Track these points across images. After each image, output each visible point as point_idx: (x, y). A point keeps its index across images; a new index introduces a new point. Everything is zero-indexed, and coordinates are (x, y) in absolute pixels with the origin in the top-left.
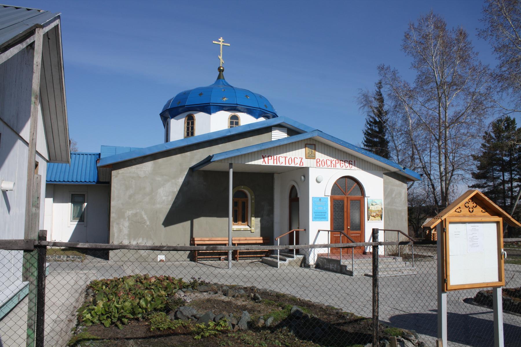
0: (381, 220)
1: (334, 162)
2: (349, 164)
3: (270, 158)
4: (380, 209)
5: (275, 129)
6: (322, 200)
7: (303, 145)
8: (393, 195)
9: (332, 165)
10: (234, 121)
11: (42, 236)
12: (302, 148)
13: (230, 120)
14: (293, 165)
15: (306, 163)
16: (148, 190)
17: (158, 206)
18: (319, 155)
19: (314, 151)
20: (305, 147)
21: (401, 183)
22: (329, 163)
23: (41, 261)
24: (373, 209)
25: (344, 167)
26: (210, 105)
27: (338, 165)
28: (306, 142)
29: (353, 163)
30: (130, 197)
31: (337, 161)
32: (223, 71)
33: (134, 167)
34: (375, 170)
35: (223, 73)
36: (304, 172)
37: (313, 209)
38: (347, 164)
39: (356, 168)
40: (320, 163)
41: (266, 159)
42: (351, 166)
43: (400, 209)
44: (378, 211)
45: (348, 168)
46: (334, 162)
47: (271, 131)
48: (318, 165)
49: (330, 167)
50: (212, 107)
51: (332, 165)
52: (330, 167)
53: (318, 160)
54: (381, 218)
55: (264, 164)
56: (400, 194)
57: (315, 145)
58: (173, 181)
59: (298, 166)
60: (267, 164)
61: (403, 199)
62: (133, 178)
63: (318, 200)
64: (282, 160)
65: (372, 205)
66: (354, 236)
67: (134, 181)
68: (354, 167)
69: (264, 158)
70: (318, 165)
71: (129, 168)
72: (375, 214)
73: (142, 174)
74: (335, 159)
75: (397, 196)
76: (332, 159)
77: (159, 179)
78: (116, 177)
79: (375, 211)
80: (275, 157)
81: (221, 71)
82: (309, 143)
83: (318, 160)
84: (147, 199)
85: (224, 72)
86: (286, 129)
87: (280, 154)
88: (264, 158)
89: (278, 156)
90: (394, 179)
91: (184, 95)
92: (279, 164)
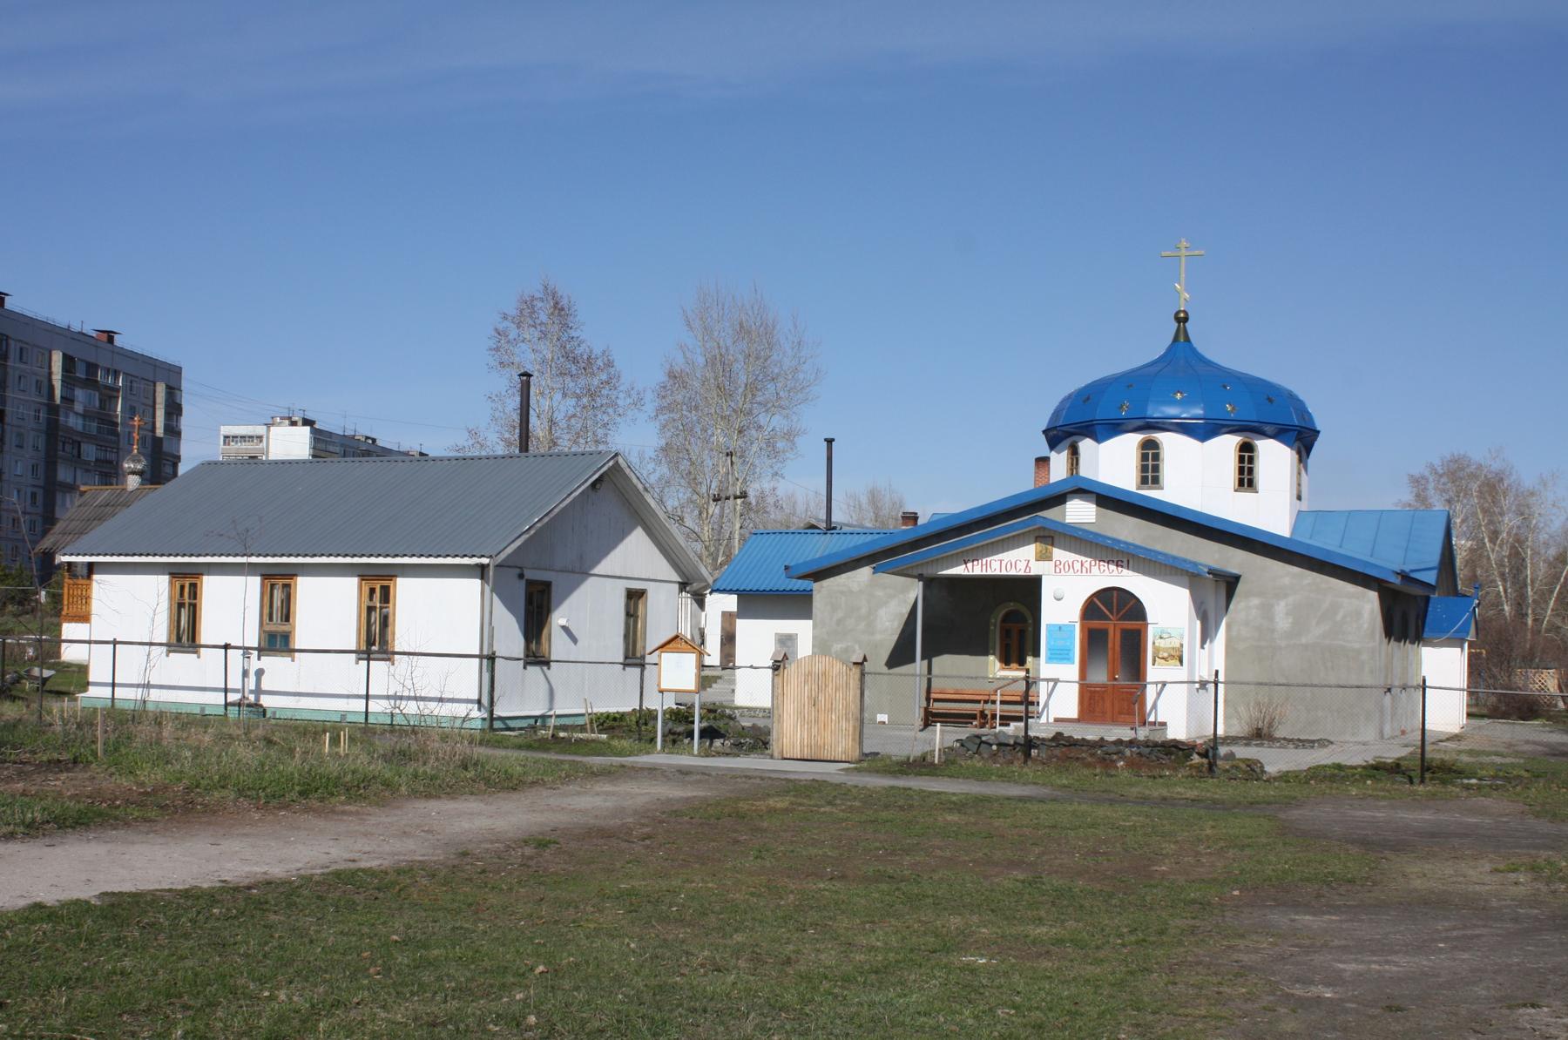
0: (1182, 664)
1: (1087, 565)
2: (1117, 566)
3: (976, 563)
4: (1178, 646)
5: (1072, 499)
6: (1063, 628)
7: (1033, 539)
8: (1339, 618)
9: (1084, 569)
10: (1150, 452)
11: (494, 653)
12: (1029, 544)
13: (1140, 451)
14: (1013, 572)
15: (1036, 569)
16: (864, 611)
17: (878, 637)
18: (1058, 553)
19: (1050, 547)
20: (1036, 541)
21: (1360, 589)
22: (1077, 566)
23: (493, 663)
24: (1162, 645)
25: (1107, 572)
26: (1093, 425)
27: (1095, 570)
28: (1037, 534)
29: (1125, 563)
30: (839, 622)
31: (1093, 563)
32: (1186, 319)
33: (844, 576)
34: (1171, 574)
35: (1187, 324)
36: (1030, 587)
37: (1047, 643)
38: (1112, 567)
39: (1131, 573)
40: (1062, 566)
41: (970, 565)
42: (1120, 569)
43: (1357, 646)
44: (1173, 648)
45: (1115, 573)
46: (1087, 565)
47: (1064, 502)
48: (1058, 570)
49: (1079, 573)
50: (1098, 429)
51: (1084, 569)
52: (1079, 573)
53: (1058, 563)
54: (1181, 662)
55: (966, 573)
56: (1358, 614)
57: (1052, 537)
58: (901, 596)
59: (1022, 573)
60: (971, 573)
61: (1366, 626)
62: (842, 593)
63: (1057, 628)
64: (996, 565)
65: (1161, 638)
66: (1127, 692)
67: (843, 598)
68: (1125, 571)
69: (966, 563)
70: (1058, 570)
71: (837, 578)
72: (1166, 655)
73: (855, 587)
74: (1089, 560)
75: (1348, 619)
76: (1084, 559)
77: (880, 593)
78: (819, 591)
79: (1165, 650)
80: (984, 560)
81: (1182, 319)
82: (1042, 534)
83: (1058, 563)
84: (862, 626)
85: (1189, 322)
86: (1094, 496)
87: (993, 555)
88: (966, 563)
89: (989, 559)
90: (1342, 582)
91: (1087, 395)
92: (989, 573)
